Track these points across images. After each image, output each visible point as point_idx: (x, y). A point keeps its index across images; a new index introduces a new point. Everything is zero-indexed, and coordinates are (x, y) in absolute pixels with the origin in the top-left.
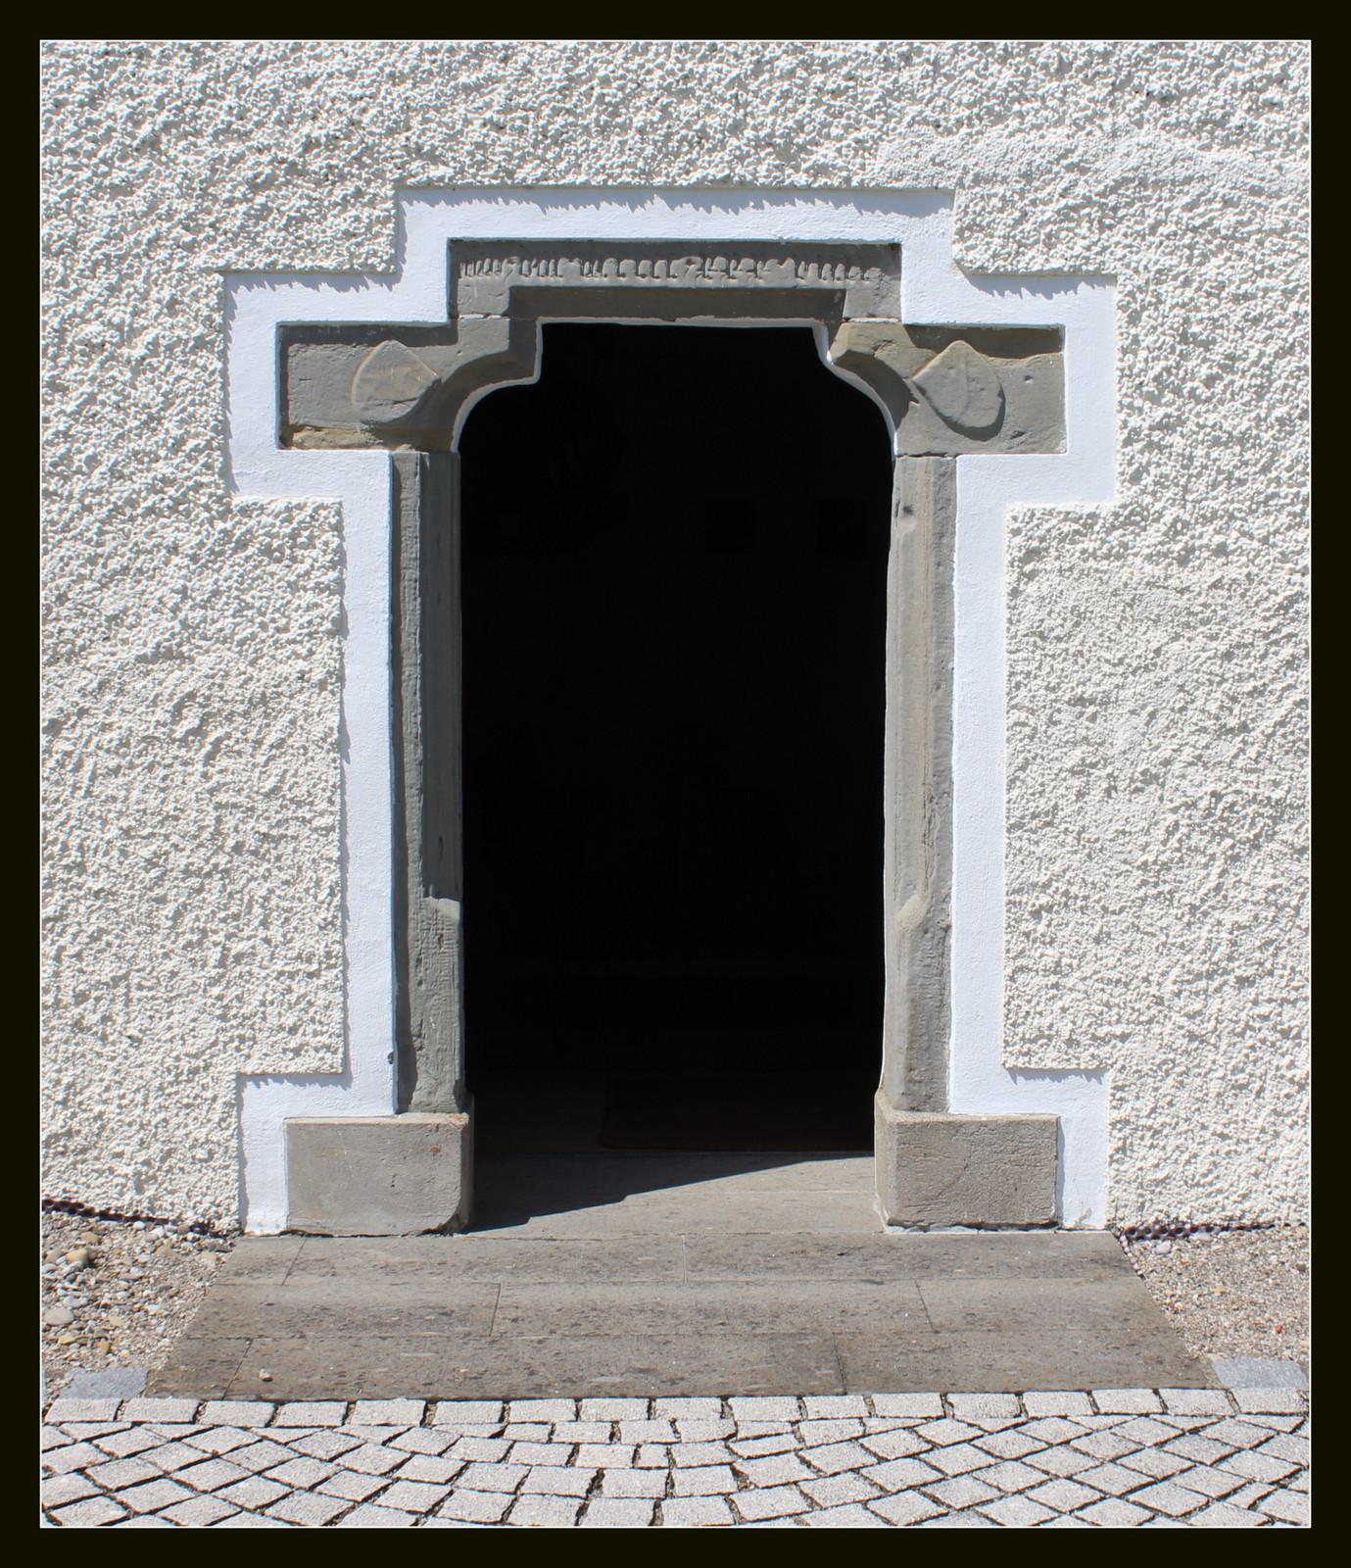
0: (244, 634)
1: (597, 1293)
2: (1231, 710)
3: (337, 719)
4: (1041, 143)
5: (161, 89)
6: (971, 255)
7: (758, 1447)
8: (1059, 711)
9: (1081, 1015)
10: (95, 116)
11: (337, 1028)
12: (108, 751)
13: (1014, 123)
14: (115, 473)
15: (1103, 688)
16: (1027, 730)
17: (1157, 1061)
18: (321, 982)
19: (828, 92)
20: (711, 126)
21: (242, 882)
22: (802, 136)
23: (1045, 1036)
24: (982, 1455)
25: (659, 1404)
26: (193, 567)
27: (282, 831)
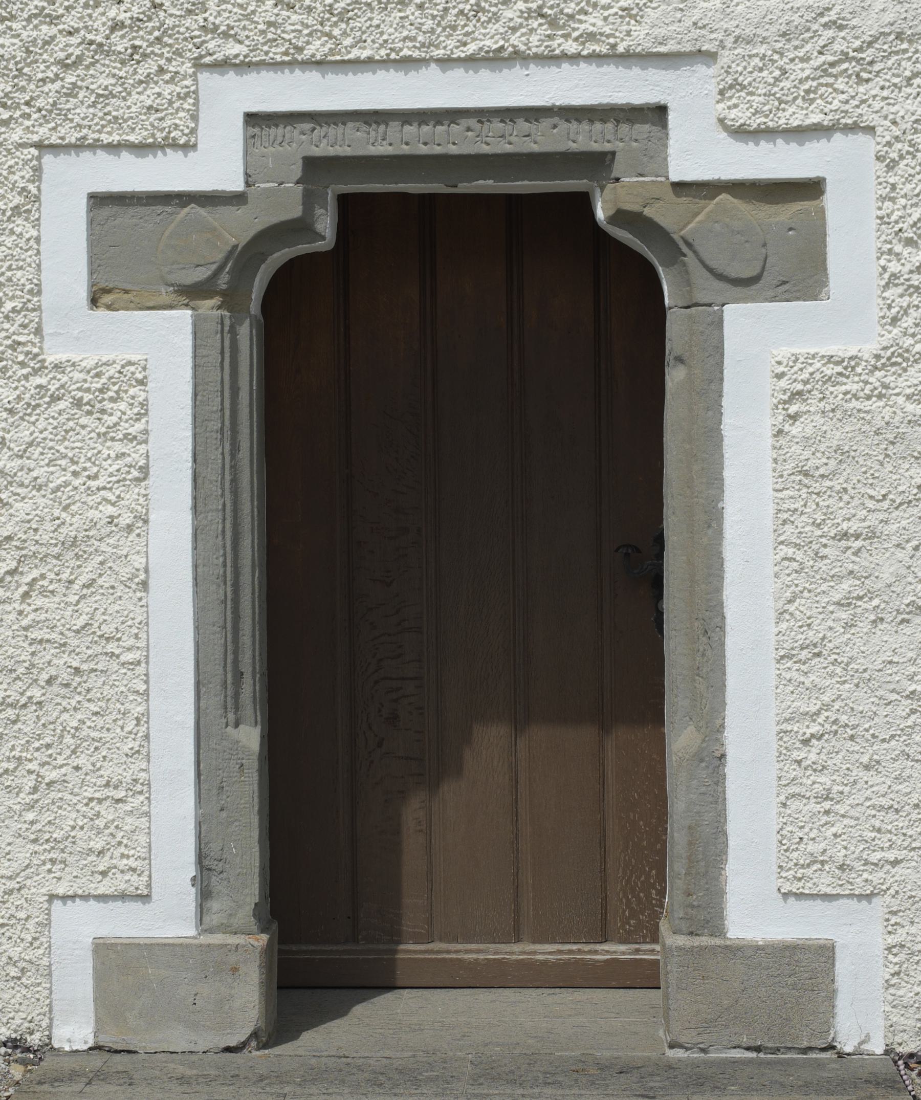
0: (59, 482)
3: (144, 560)
6: (733, 113)
8: (825, 546)
9: (854, 841)
11: (143, 852)
15: (867, 523)
16: (795, 565)
18: (128, 808)
21: (55, 714)
26: (11, 420)
27: (92, 665)
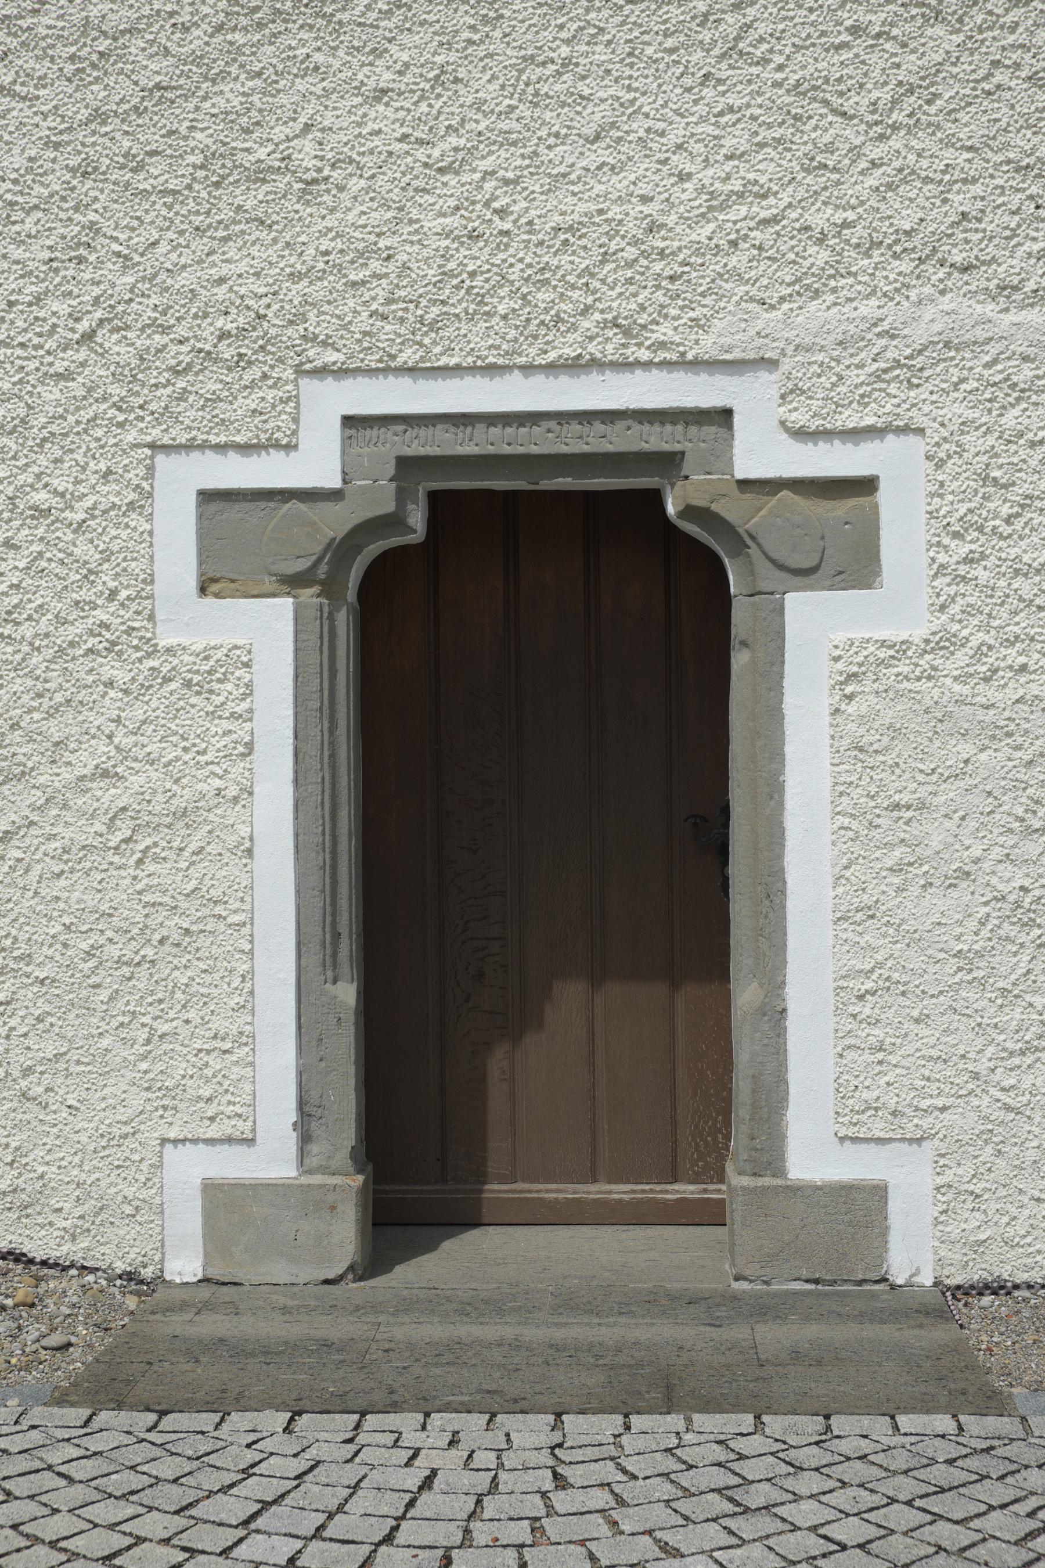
0: (170, 757)
1: (465, 1331)
2: (1035, 812)
3: (249, 829)
4: (854, 314)
5: (96, 291)
6: (794, 416)
7: (578, 1455)
8: (879, 816)
10: (42, 314)
11: (248, 1099)
12: (53, 858)
13: (830, 298)
14: (61, 621)
15: (918, 795)
16: (851, 834)
17: (977, 1132)
19: (666, 278)
20: (565, 312)
21: (167, 971)
22: (645, 316)
23: (873, 1108)
24: (783, 1465)
25: (500, 1418)
26: (126, 700)
27: (201, 927)
